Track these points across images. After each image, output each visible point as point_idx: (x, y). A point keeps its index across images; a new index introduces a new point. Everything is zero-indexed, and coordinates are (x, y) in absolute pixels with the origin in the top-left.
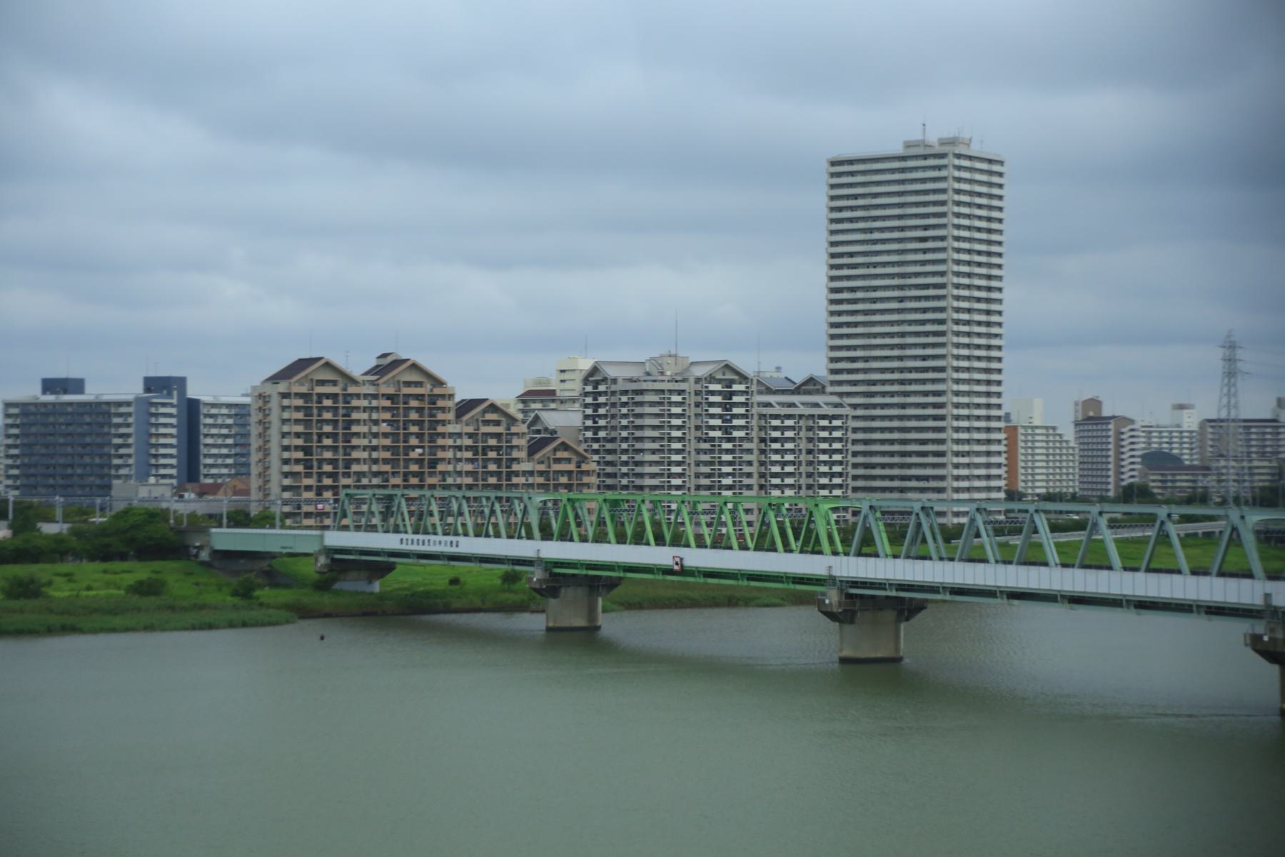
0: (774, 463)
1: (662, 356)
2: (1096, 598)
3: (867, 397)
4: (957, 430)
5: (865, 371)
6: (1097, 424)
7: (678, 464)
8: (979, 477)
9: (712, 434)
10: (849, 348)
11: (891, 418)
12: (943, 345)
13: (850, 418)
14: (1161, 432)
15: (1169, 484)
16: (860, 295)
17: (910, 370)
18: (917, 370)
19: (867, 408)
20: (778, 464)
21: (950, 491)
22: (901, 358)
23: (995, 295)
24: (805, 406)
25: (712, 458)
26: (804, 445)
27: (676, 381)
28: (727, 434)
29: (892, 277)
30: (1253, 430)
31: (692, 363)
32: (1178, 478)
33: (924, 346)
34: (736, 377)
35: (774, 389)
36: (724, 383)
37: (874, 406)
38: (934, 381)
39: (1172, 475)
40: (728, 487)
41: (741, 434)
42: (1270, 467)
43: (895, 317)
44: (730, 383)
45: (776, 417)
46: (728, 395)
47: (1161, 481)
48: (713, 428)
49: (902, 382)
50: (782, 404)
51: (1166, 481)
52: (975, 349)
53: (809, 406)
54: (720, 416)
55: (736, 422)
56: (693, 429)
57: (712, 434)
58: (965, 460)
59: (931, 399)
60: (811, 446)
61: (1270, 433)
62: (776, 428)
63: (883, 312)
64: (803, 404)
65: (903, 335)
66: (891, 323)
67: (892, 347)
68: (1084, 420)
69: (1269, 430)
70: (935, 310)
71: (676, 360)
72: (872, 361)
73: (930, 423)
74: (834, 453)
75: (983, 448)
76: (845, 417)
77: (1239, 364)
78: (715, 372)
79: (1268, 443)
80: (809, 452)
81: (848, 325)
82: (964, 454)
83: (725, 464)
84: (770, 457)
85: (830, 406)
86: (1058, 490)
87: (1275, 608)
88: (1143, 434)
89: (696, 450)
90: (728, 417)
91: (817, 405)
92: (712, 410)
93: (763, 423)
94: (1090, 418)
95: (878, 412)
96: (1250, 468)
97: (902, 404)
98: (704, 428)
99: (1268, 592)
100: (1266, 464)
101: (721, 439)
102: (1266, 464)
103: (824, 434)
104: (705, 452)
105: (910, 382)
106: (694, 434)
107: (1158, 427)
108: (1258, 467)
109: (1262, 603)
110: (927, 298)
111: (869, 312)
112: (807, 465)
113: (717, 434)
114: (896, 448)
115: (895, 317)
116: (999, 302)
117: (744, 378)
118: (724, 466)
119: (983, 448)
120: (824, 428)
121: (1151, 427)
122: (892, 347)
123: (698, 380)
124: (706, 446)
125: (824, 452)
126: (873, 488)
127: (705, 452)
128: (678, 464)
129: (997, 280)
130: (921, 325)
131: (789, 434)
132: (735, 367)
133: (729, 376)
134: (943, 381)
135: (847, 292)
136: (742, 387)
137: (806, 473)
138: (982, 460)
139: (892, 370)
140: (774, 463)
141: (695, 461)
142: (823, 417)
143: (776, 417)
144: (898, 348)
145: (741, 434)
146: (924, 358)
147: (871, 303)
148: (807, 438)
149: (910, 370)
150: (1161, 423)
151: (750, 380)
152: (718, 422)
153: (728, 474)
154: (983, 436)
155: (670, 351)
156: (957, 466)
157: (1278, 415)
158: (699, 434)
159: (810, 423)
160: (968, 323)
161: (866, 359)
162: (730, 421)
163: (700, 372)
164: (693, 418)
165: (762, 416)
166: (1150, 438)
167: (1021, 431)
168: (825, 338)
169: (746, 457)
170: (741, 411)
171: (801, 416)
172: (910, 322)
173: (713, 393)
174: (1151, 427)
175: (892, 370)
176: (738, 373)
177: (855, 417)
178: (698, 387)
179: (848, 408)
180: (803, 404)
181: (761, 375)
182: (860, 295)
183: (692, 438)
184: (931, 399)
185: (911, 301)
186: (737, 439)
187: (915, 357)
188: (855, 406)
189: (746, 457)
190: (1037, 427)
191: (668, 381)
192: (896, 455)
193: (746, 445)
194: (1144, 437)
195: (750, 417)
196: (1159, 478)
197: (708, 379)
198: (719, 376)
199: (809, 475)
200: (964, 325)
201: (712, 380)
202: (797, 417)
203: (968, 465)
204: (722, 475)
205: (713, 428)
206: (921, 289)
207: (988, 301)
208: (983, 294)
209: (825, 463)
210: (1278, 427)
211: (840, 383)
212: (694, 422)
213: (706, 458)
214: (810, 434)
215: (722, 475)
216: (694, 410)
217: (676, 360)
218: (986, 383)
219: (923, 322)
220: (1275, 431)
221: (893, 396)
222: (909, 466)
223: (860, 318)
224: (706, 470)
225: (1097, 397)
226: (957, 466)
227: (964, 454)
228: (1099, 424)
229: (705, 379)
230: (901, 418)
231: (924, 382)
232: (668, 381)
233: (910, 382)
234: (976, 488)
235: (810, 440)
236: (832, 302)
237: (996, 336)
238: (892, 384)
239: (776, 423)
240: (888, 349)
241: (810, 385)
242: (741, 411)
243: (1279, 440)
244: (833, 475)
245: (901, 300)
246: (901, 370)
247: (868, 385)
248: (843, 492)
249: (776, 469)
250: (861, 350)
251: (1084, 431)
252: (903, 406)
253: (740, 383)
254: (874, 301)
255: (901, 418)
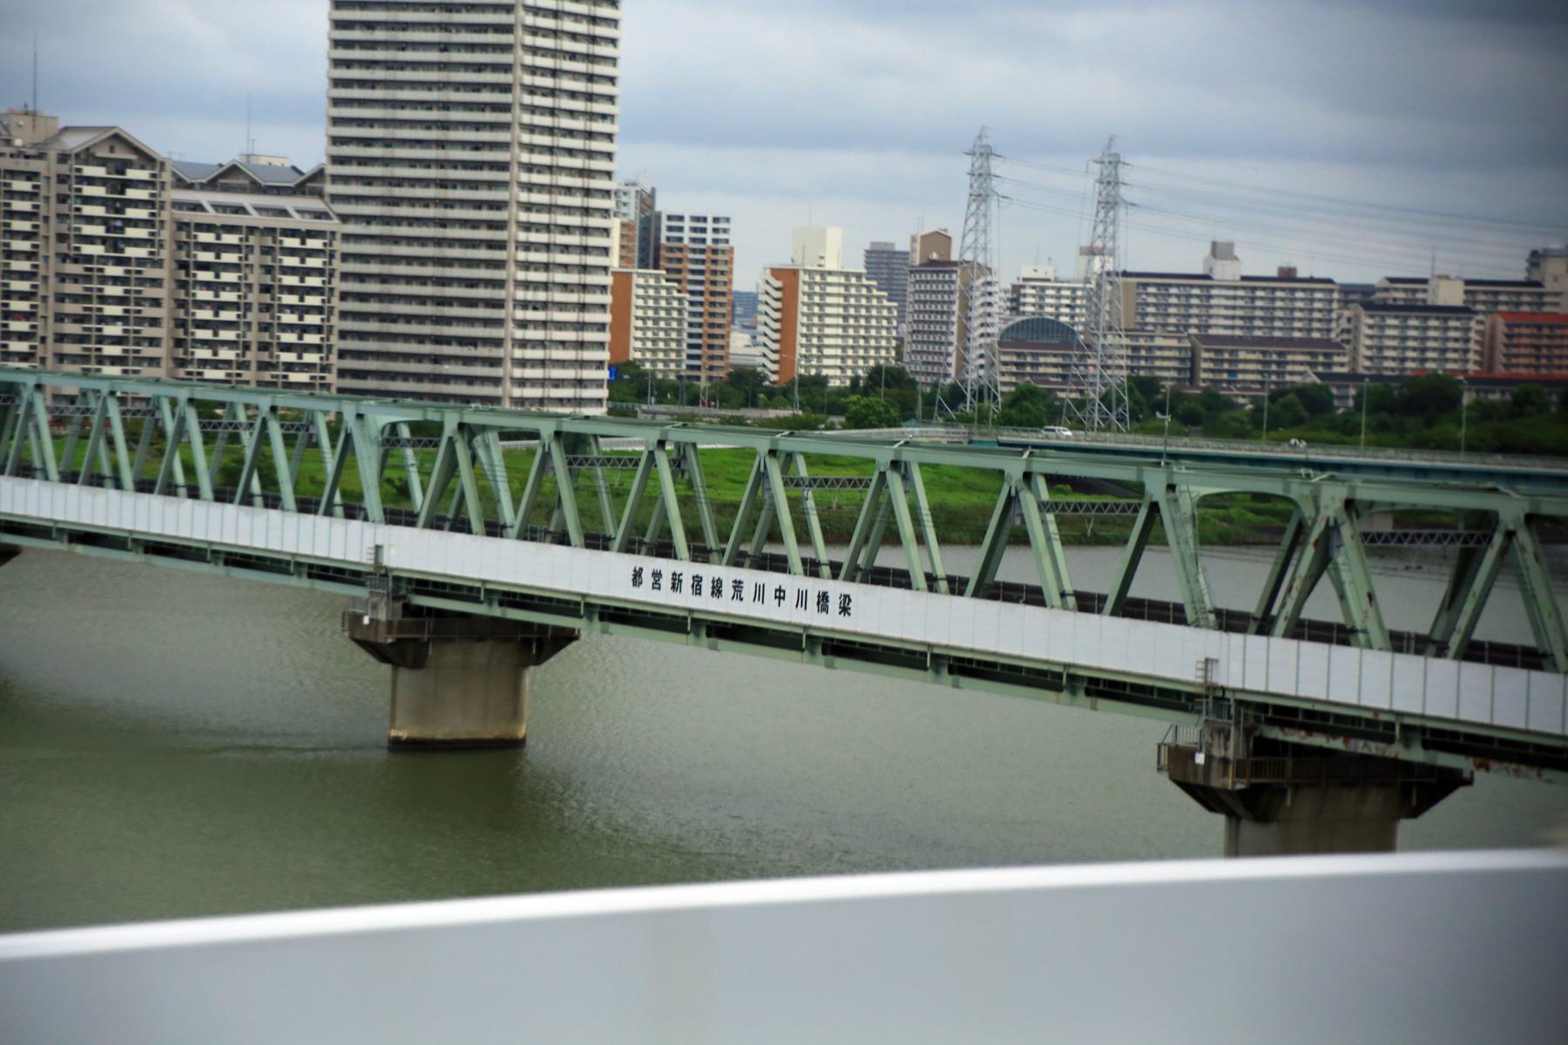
0: (201, 304)
1: (12, 113)
2: (189, 548)
3: (389, 204)
4: (526, 266)
5: (386, 162)
6: (938, 272)
7: (23, 296)
8: (563, 344)
9: (87, 249)
10: (361, 122)
11: (422, 241)
12: (505, 126)
13: (338, 237)
14: (1059, 289)
15: (1028, 369)
16: (379, 35)
17: (455, 164)
18: (466, 165)
19: (388, 224)
20: (209, 307)
21: (508, 364)
22: (441, 144)
23: (602, 50)
24: (264, 213)
25: (86, 289)
26: (255, 278)
27: (27, 157)
28: (116, 251)
29: (431, 8)
30: (1173, 291)
31: (66, 129)
32: (1042, 360)
33: (478, 126)
34: (133, 157)
35: (263, 183)
36: (110, 165)
37: (399, 221)
38: (491, 185)
39: (1033, 355)
40: (115, 340)
41: (141, 252)
42: (1180, 349)
43: (433, 76)
44: (122, 166)
45: (209, 228)
46: (119, 187)
47: (1016, 364)
48: (90, 240)
49: (443, 184)
50: (218, 207)
51: (1023, 365)
52: (564, 136)
53: (270, 213)
54: (104, 221)
55: (131, 232)
56: (53, 240)
57: (87, 249)
58: (540, 315)
59: (485, 214)
60: (267, 280)
61: (1198, 296)
62: (206, 247)
63: (415, 65)
64: (300, 211)
65: (446, 106)
66: (429, 85)
67: (428, 125)
68: (921, 265)
69: (1196, 291)
70: (496, 68)
71: (34, 121)
72: (397, 147)
73: (483, 254)
74: (308, 294)
75: (573, 298)
76: (328, 235)
77: (1123, 190)
78: (95, 145)
79: (1194, 311)
80: (266, 289)
81: (362, 83)
82: (536, 306)
83: (110, 301)
84: (194, 295)
85: (307, 216)
86: (813, 372)
87: (387, 569)
88: (1033, 292)
89: (57, 275)
90: (119, 224)
91: (283, 213)
92: (88, 210)
93: (183, 236)
94: (933, 263)
95: (404, 231)
96: (1149, 349)
97: (440, 219)
98: (72, 239)
99: (379, 543)
100: (1174, 343)
101: (104, 260)
102: (1174, 343)
103: (292, 261)
104: (75, 279)
105: (454, 184)
106: (54, 247)
107: (1056, 280)
108: (1160, 348)
109: (372, 562)
110: (484, 47)
111: (395, 65)
112: (261, 310)
113: (97, 250)
114: (429, 290)
115: (433, 76)
116: (611, 62)
117: (147, 160)
118: (109, 304)
119: (573, 298)
120: (292, 252)
121: (1049, 280)
122: (428, 125)
123: (63, 158)
124: (77, 269)
125: (291, 290)
126: (393, 353)
127: (75, 279)
128: (23, 296)
129: (609, 26)
130: (474, 91)
131: (229, 258)
132: (133, 141)
133: (121, 154)
134: (504, 185)
135: (361, 29)
136: (143, 175)
137: (259, 323)
138: (571, 316)
139: (427, 163)
140: (201, 304)
141: (56, 294)
142: (293, 233)
143: (209, 228)
144: (438, 128)
145: (141, 252)
146: (477, 146)
147: (398, 49)
148: (262, 266)
149: (455, 164)
150: (1062, 275)
151: (158, 165)
152: (99, 230)
153: (114, 319)
154: (573, 278)
155: (26, 106)
156: (523, 324)
157: (1211, 270)
158: (63, 248)
159: (268, 241)
160: (552, 92)
161: (388, 143)
162: (121, 230)
163: (73, 143)
164: (53, 220)
165: (182, 226)
166: (1042, 298)
167: (804, 277)
168: (324, 103)
169: (149, 292)
170: (142, 214)
171: (252, 230)
172: (458, 86)
173: (91, 181)
174: (1049, 280)
175: (427, 163)
176: (136, 150)
177: (347, 237)
178: (64, 169)
179: (336, 221)
180: (300, 211)
181: (253, 161)
182: (379, 35)
183: (52, 254)
184: (485, 214)
185: (459, 51)
186: (133, 262)
187: (463, 144)
188: (345, 218)
189: (149, 292)
190: (830, 273)
191: (12, 156)
192: (428, 302)
193: (149, 272)
194: (1034, 296)
195: (158, 225)
196: (1060, 360)
197: (83, 156)
198: (103, 153)
199: (265, 327)
200: (544, 95)
201: (91, 159)
202: (244, 230)
203: (544, 324)
204: (104, 319)
205: (90, 240)
206: (476, 32)
207: (591, 58)
208: (581, 47)
209: (293, 309)
210: (1541, 295)
211: (346, 179)
212: (54, 227)
213: (76, 289)
214: (268, 260)
215: (104, 319)
216: (54, 208)
217: (34, 121)
218: (583, 192)
219: (477, 87)
220: (1205, 293)
221: (427, 206)
222: (448, 321)
223: (379, 74)
224: (76, 309)
225: (945, 230)
226: (523, 324)
227: (536, 306)
228: (940, 271)
229: (77, 155)
230: (439, 242)
231: (474, 185)
232: (12, 156)
233: (454, 184)
234: (558, 361)
235: (268, 270)
236: (337, 44)
237: (604, 117)
238: (427, 186)
239: (207, 237)
240: (422, 128)
241: (308, 185)
242: (142, 214)
243: (1211, 307)
244: (304, 329)
245: (445, 47)
246: (441, 164)
247: (390, 185)
248: (321, 358)
249: (205, 314)
250: (379, 127)
251: (921, 282)
252: (443, 223)
253: (142, 168)
254: (403, 46)
255: (439, 242)
